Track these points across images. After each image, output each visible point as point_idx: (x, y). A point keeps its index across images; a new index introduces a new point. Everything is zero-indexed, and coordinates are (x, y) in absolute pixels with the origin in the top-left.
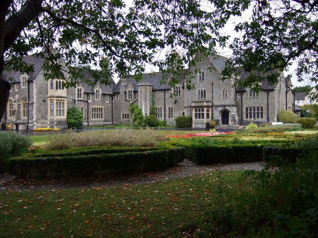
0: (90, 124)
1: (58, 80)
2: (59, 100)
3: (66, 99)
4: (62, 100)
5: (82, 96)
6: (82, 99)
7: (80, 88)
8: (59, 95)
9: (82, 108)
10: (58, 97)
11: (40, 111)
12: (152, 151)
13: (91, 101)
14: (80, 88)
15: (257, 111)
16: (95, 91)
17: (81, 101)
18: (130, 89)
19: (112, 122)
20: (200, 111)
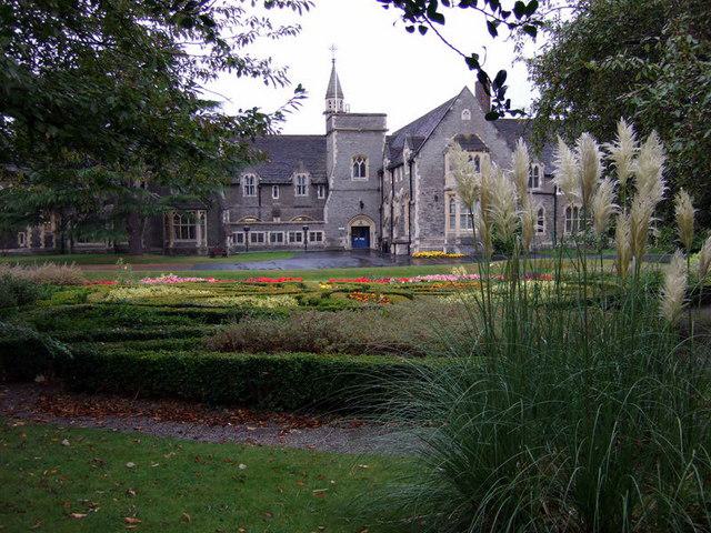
5: (540, 183)
6: (539, 189)
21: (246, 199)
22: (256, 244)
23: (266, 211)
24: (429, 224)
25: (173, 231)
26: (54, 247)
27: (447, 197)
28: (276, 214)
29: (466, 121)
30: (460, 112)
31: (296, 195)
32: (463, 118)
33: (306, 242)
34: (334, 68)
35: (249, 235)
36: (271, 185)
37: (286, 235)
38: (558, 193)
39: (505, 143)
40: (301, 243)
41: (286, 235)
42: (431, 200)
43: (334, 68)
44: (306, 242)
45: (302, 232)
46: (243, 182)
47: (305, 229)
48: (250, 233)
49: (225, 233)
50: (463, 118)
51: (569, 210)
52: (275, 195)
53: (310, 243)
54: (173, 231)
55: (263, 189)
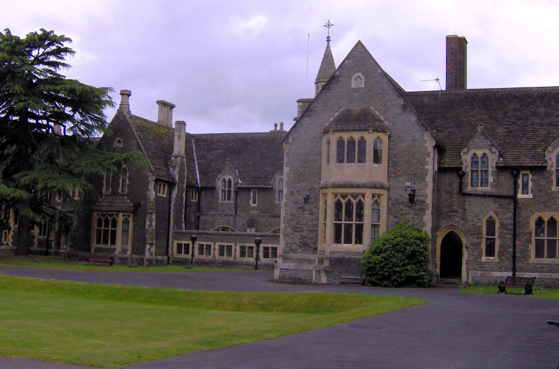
0: (518, 274)
1: (346, 136)
2: (344, 196)
3: (385, 192)
4: (355, 196)
5: (491, 179)
6: (488, 189)
7: (479, 153)
8: (345, 179)
9: (491, 223)
10: (345, 186)
11: (296, 229)
12: (251, 340)
13: (530, 196)
14: (479, 153)
15: (105, 227)
16: (466, 158)
17: (484, 196)
18: (227, 178)
19: (514, 270)
20: (107, 225)
21: (222, 205)
22: (203, 257)
23: (242, 220)
24: (298, 235)
25: (94, 235)
26: (35, 246)
27: (321, 197)
28: (252, 223)
29: (357, 90)
30: (350, 78)
31: (220, 201)
32: (354, 85)
33: (257, 258)
34: (328, 47)
35: (196, 246)
36: (249, 189)
37: (237, 249)
38: (520, 196)
39: (414, 119)
40: (252, 260)
41: (237, 249)
42: (300, 199)
43: (328, 47)
44: (257, 258)
45: (190, 242)
46: (219, 184)
47: (194, 240)
48: (197, 243)
49: (145, 239)
50: (354, 85)
51: (540, 222)
52: (254, 202)
53: (263, 260)
54: (94, 235)
55: (240, 193)
